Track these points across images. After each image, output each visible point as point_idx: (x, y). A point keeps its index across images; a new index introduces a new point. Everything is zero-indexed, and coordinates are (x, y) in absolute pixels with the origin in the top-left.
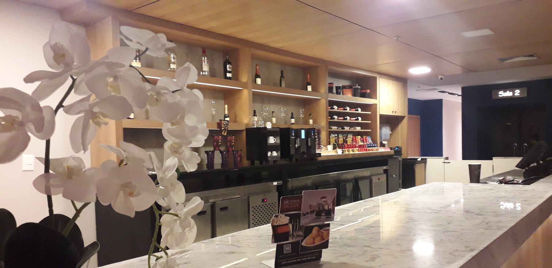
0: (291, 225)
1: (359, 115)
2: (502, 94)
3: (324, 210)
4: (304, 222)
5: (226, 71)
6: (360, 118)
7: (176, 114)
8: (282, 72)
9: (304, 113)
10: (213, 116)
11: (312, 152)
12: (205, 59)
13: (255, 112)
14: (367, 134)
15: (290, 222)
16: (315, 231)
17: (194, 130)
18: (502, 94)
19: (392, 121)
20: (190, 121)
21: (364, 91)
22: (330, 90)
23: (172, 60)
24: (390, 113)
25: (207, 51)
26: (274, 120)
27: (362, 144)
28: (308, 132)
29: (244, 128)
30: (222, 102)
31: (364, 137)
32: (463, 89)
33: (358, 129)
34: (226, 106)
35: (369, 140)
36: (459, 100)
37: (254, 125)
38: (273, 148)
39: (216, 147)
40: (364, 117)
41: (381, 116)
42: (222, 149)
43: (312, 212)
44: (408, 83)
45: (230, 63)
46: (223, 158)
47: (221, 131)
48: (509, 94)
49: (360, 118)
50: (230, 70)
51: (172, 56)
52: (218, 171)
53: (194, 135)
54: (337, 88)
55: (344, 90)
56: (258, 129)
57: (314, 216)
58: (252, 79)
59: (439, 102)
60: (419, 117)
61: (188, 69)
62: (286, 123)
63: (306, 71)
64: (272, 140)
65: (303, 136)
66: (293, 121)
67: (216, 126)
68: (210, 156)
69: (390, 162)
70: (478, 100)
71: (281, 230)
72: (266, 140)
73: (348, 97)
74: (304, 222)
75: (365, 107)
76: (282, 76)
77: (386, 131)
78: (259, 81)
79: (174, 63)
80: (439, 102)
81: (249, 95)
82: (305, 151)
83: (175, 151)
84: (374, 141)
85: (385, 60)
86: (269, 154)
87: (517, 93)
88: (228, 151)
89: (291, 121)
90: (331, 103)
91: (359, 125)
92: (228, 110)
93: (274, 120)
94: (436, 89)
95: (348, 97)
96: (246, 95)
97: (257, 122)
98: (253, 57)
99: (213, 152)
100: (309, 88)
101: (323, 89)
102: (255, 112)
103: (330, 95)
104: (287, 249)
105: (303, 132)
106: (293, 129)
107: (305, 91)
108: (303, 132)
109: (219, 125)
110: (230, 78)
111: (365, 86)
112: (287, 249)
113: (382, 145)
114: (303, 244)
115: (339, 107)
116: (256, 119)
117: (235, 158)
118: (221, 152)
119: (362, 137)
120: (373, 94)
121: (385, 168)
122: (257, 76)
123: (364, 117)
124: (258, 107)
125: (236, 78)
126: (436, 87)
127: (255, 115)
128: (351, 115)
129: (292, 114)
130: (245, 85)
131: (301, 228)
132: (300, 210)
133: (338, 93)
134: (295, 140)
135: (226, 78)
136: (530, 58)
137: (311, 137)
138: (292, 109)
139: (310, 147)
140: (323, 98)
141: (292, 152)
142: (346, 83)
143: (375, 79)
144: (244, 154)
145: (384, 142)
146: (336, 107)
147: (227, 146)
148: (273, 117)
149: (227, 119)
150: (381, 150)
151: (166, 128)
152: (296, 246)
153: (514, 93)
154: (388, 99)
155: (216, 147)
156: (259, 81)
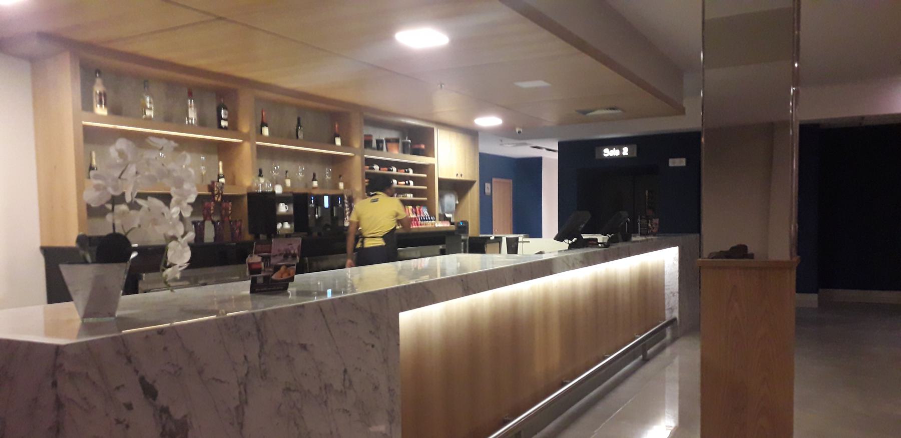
0: (263, 264)
1: (411, 178)
2: (608, 153)
3: (290, 254)
4: (273, 261)
5: (220, 118)
6: (411, 182)
7: (179, 183)
8: (299, 119)
9: (332, 174)
10: (202, 175)
11: (340, 224)
12: (191, 103)
13: (260, 171)
14: (421, 204)
15: (262, 260)
16: (282, 269)
17: (189, 192)
18: (608, 153)
19: (458, 188)
20: (186, 186)
21: (416, 146)
22: (368, 143)
23: (148, 105)
24: (454, 177)
25: (194, 93)
26: (288, 182)
27: (414, 216)
28: (333, 200)
29: (245, 192)
30: (216, 157)
31: (417, 208)
32: (560, 144)
33: (410, 196)
34: (221, 164)
35: (425, 212)
36: (555, 156)
37: (258, 188)
38: (284, 218)
39: (207, 216)
40: (417, 181)
41: (441, 181)
42: (215, 219)
43: (280, 254)
44: (480, 134)
45: (225, 108)
46: (216, 230)
47: (213, 196)
48: (615, 153)
49: (411, 182)
50: (226, 117)
51: (148, 99)
52: (209, 245)
53: (189, 195)
54: (379, 142)
55: (389, 145)
56: (264, 194)
57: (282, 257)
58: (257, 128)
59: (539, 160)
60: (511, 181)
61: (185, 157)
62: (306, 186)
63: (331, 119)
64: (283, 208)
65: (326, 205)
66: (315, 184)
67: (206, 189)
68: (199, 230)
69: (447, 240)
70: (577, 157)
71: (254, 267)
72: (274, 209)
73: (395, 155)
74: (273, 261)
75: (417, 168)
76: (299, 124)
77: (450, 200)
78: (266, 131)
79: (150, 109)
80: (539, 160)
81: (252, 148)
82: (330, 223)
83: (178, 203)
84: (431, 213)
85: (446, 104)
86: (279, 226)
87: (625, 151)
88: (222, 222)
89: (312, 183)
90: (369, 162)
91: (411, 191)
92: (224, 169)
93: (288, 182)
94: (525, 144)
95: (395, 155)
96: (247, 149)
97: (263, 185)
98: (258, 100)
99: (203, 223)
100: (338, 142)
101: (357, 144)
102: (260, 171)
103: (368, 150)
104: (260, 281)
105: (326, 199)
106: (311, 195)
107: (330, 146)
108: (326, 199)
109: (211, 188)
110: (226, 128)
111: (419, 140)
112: (260, 281)
113: (443, 218)
114: (274, 277)
115: (380, 167)
116: (262, 180)
117: (232, 230)
118: (214, 223)
119: (414, 207)
120: (428, 151)
121: (441, 247)
122: (264, 124)
123: (417, 181)
124: (265, 164)
125: (233, 128)
126: (527, 142)
127: (260, 175)
128: (400, 178)
129: (314, 175)
130: (246, 138)
131: (271, 266)
132: (270, 252)
133: (379, 148)
134: (315, 209)
135: (220, 127)
136: (613, 112)
137: (337, 205)
138: (315, 168)
139: (337, 218)
140: (356, 156)
141: (311, 224)
142: (393, 135)
143: (433, 130)
144: (245, 225)
145: (447, 215)
146: (376, 167)
147: (221, 216)
148: (286, 178)
149: (222, 180)
150: (440, 225)
151: (173, 191)
152: (266, 279)
153: (621, 151)
154: (450, 158)
155: (207, 216)
156: (266, 131)
